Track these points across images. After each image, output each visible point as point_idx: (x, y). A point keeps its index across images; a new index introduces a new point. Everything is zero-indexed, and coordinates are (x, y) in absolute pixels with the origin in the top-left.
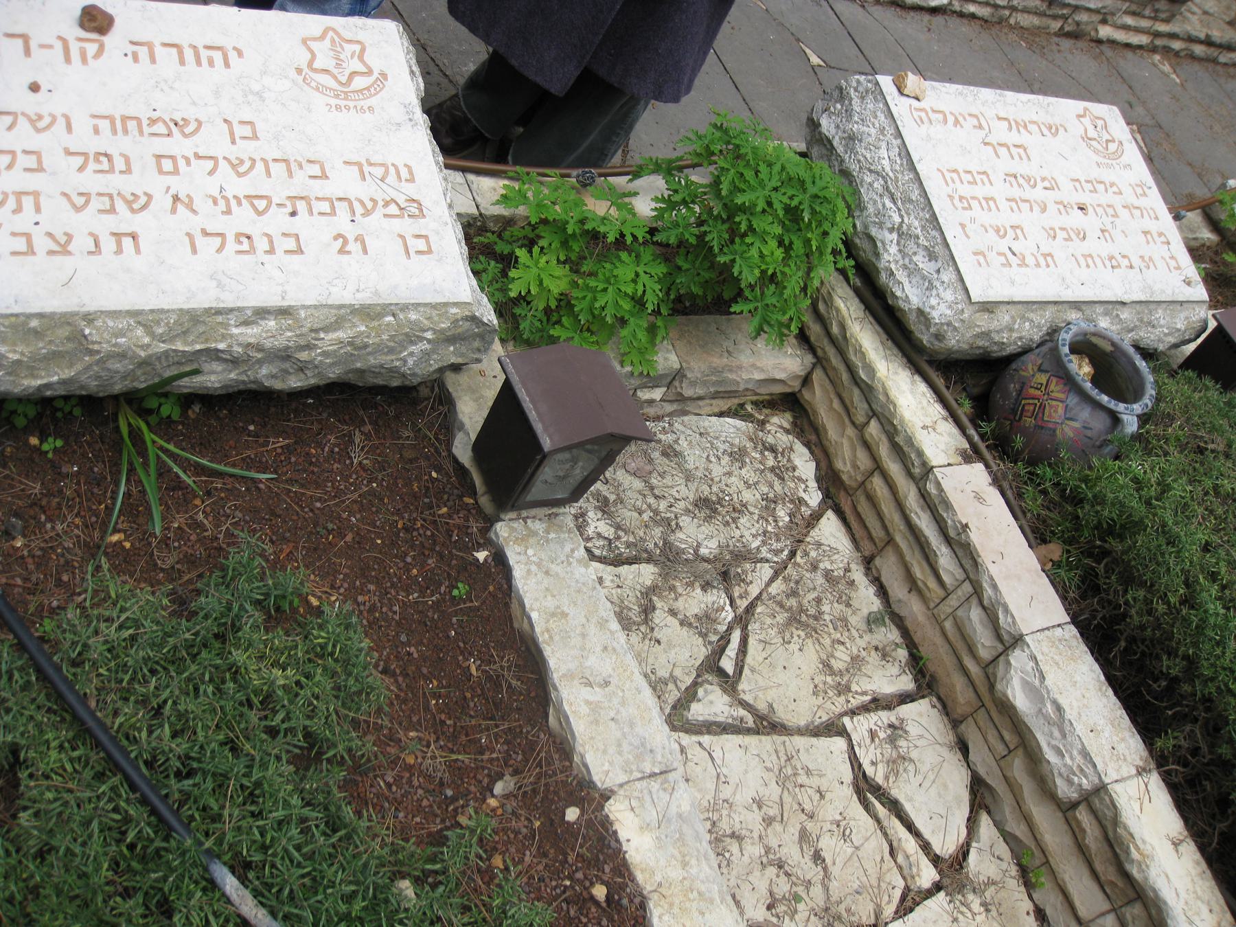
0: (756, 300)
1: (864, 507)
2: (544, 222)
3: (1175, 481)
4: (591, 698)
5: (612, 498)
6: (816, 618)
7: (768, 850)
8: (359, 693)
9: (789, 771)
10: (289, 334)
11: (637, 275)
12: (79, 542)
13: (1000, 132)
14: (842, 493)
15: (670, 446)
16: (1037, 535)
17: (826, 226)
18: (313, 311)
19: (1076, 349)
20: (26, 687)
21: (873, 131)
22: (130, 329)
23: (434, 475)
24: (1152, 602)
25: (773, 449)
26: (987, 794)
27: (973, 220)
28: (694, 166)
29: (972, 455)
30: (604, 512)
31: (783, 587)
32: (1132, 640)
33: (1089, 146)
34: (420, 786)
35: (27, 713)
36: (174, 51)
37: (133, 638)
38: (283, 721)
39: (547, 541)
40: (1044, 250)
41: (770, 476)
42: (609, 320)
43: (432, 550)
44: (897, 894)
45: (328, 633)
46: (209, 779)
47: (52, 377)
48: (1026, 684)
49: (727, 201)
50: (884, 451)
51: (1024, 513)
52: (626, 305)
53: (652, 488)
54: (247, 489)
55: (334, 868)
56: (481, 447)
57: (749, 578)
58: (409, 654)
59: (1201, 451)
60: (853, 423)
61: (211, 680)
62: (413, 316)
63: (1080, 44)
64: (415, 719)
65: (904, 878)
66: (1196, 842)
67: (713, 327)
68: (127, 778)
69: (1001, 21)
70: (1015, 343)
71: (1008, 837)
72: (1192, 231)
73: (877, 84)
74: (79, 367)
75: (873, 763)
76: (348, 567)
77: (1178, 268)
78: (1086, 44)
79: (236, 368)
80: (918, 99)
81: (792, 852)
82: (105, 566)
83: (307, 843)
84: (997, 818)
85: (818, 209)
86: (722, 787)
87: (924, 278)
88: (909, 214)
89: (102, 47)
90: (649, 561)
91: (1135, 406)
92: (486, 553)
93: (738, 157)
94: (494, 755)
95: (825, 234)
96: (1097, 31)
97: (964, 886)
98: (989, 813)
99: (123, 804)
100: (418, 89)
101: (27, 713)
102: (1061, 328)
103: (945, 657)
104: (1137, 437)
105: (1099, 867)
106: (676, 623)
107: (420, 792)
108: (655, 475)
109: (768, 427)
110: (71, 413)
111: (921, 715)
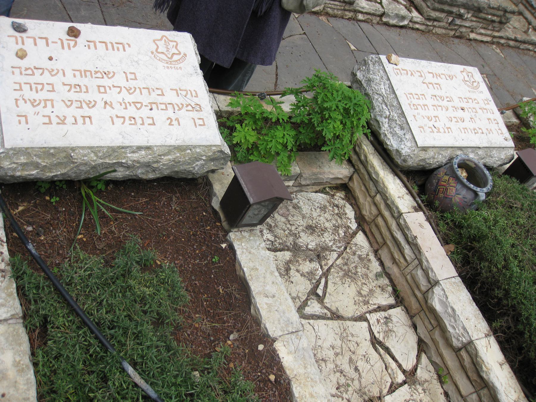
0: (331, 145)
1: (374, 230)
2: (246, 114)
3: (500, 219)
4: (268, 302)
5: (273, 225)
6: (355, 274)
7: (336, 366)
8: (178, 298)
9: (345, 335)
10: (150, 157)
11: (284, 135)
12: (66, 238)
13: (429, 78)
14: (365, 224)
15: (296, 205)
16: (445, 241)
17: (360, 116)
18: (159, 148)
19: (460, 166)
20: (50, 292)
21: (378, 78)
22: (89, 154)
23: (204, 214)
24: (491, 267)
25: (337, 206)
26: (425, 346)
27: (418, 114)
28: (306, 91)
29: (418, 209)
30: (270, 230)
31: (342, 261)
32: (483, 283)
33: (466, 84)
34: (201, 336)
35: (50, 302)
36: (104, 44)
37: (90, 275)
38: (149, 308)
39: (250, 240)
40: (447, 126)
41: (336, 217)
42: (273, 153)
43: (204, 243)
44: (388, 385)
45: (166, 274)
46: (121, 330)
47: (57, 172)
48: (440, 301)
49: (320, 106)
50: (382, 207)
51: (439, 232)
52: (280, 147)
53: (289, 221)
54: (131, 218)
55: (170, 365)
56: (223, 203)
57: (328, 258)
58: (196, 284)
59: (511, 207)
60: (370, 196)
61: (121, 292)
62: (198, 150)
63: (462, 41)
64: (198, 310)
65: (391, 378)
66: (509, 365)
67: (313, 156)
68: (90, 328)
69: (429, 31)
70: (436, 163)
71: (433, 363)
72: (509, 119)
73: (380, 58)
74: (68, 168)
75: (378, 332)
76: (172, 250)
77: (502, 134)
78: (464, 41)
79: (128, 170)
80: (396, 65)
81: (346, 367)
82: (78, 247)
83: (159, 356)
84: (429, 355)
85: (357, 109)
86: (318, 340)
87: (399, 137)
88: (392, 111)
89: (76, 43)
90: (288, 250)
91: (484, 189)
92: (225, 245)
93: (325, 88)
94: (229, 324)
95: (359, 119)
96: (469, 35)
97: (415, 382)
98: (425, 353)
99: (88, 338)
100: (198, 60)
101: (50, 302)
102: (454, 158)
103: (407, 290)
104: (485, 202)
105: (470, 374)
106: (299, 275)
107: (201, 338)
108: (290, 215)
109: (335, 197)
110: (62, 187)
111: (397, 313)
